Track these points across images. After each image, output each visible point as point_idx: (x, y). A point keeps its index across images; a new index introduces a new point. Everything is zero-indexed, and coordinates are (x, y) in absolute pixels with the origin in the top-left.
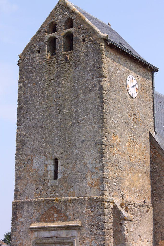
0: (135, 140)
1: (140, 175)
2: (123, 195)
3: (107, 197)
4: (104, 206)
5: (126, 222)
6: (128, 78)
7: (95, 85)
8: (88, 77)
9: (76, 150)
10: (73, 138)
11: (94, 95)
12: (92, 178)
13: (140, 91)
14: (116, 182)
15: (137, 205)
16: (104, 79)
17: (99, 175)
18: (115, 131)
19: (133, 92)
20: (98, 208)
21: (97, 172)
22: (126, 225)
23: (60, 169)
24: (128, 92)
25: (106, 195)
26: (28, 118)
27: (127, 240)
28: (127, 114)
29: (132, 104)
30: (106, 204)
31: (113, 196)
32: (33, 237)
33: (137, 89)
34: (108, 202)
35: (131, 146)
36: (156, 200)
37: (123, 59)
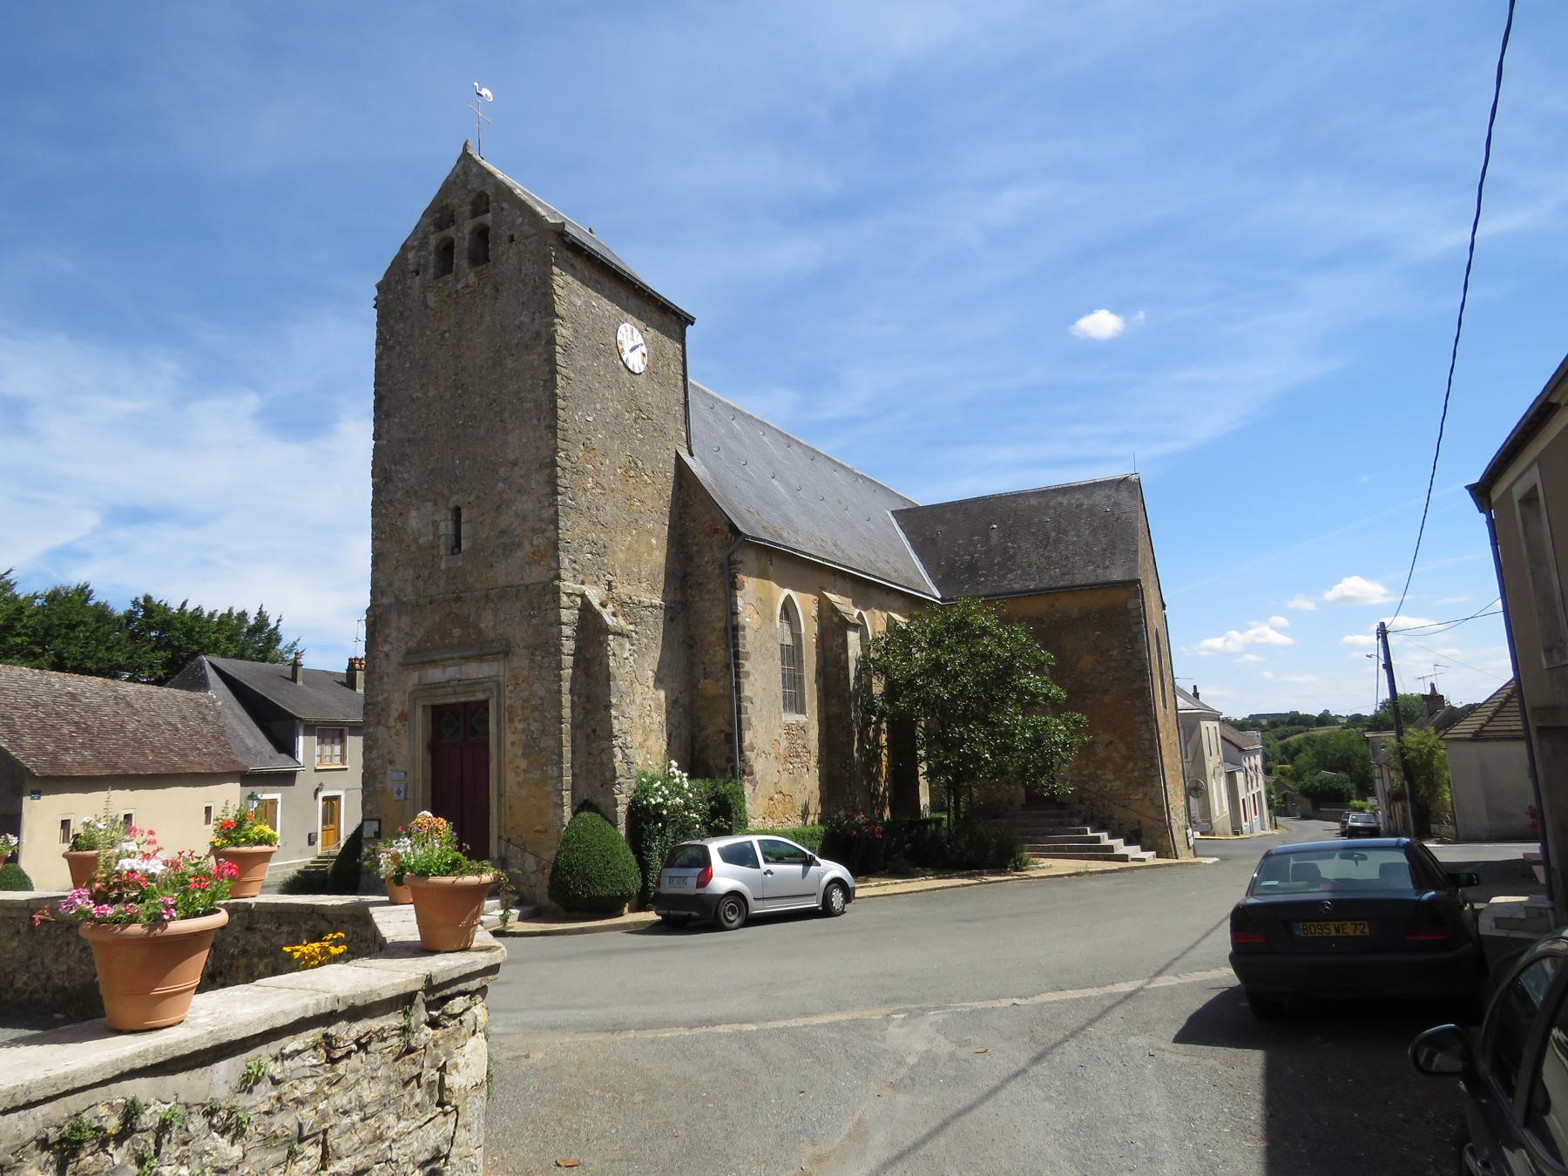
0: (640, 464)
1: (654, 541)
2: (610, 582)
3: (568, 585)
4: (559, 604)
5: (611, 637)
6: (622, 328)
7: (538, 334)
8: (522, 318)
9: (500, 484)
10: (493, 458)
11: (535, 357)
12: (535, 542)
13: (655, 358)
14: (591, 553)
15: (646, 605)
16: (556, 320)
17: (548, 534)
18: (589, 439)
19: (636, 361)
20: (546, 610)
21: (545, 530)
22: (612, 643)
23: (465, 529)
24: (622, 359)
25: (565, 580)
26: (396, 420)
27: (615, 678)
28: (619, 407)
29: (633, 387)
30: (564, 598)
31: (583, 583)
32: (411, 683)
33: (644, 355)
34: (569, 595)
35: (630, 477)
36: (692, 596)
37: (609, 285)
